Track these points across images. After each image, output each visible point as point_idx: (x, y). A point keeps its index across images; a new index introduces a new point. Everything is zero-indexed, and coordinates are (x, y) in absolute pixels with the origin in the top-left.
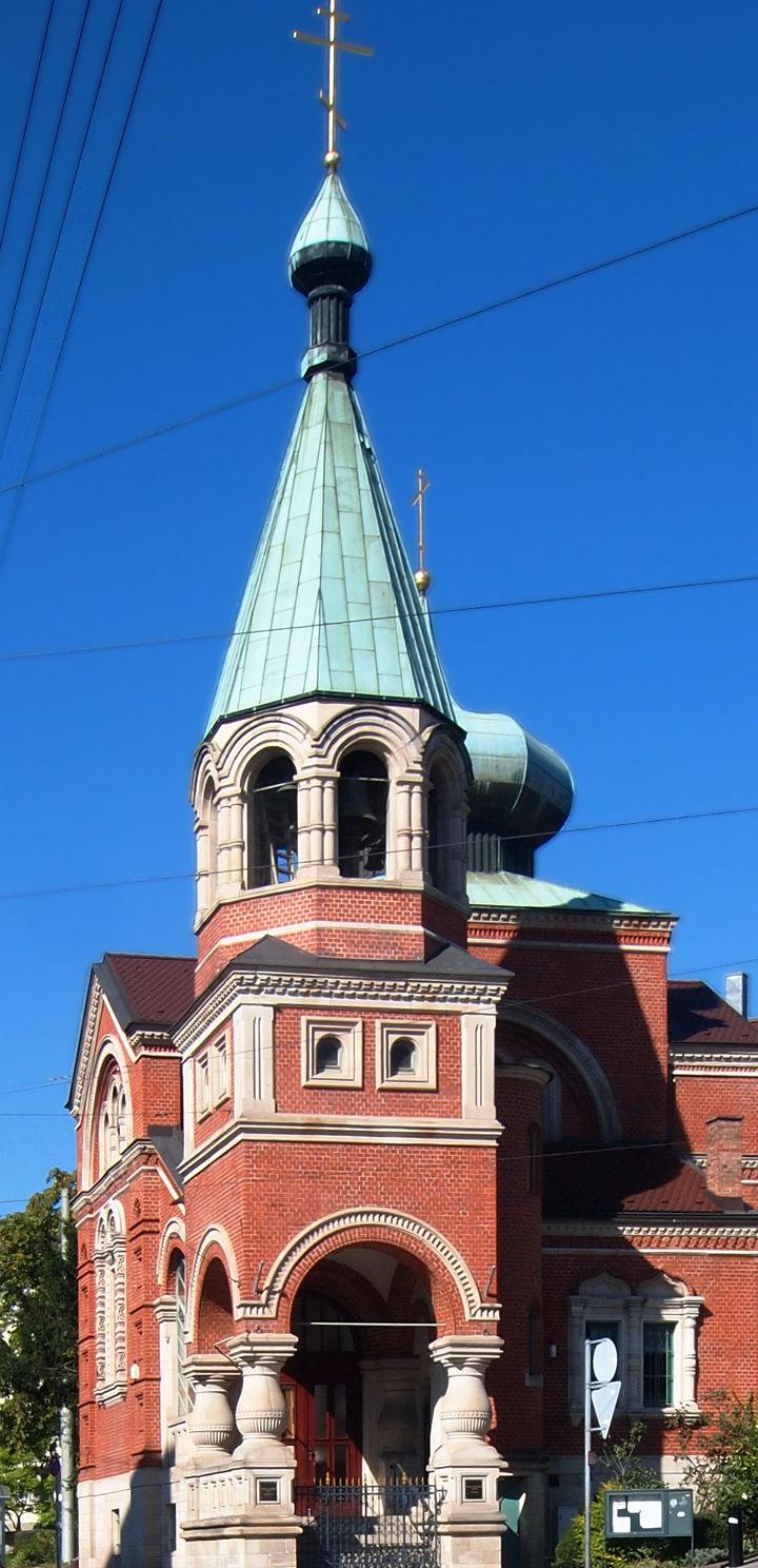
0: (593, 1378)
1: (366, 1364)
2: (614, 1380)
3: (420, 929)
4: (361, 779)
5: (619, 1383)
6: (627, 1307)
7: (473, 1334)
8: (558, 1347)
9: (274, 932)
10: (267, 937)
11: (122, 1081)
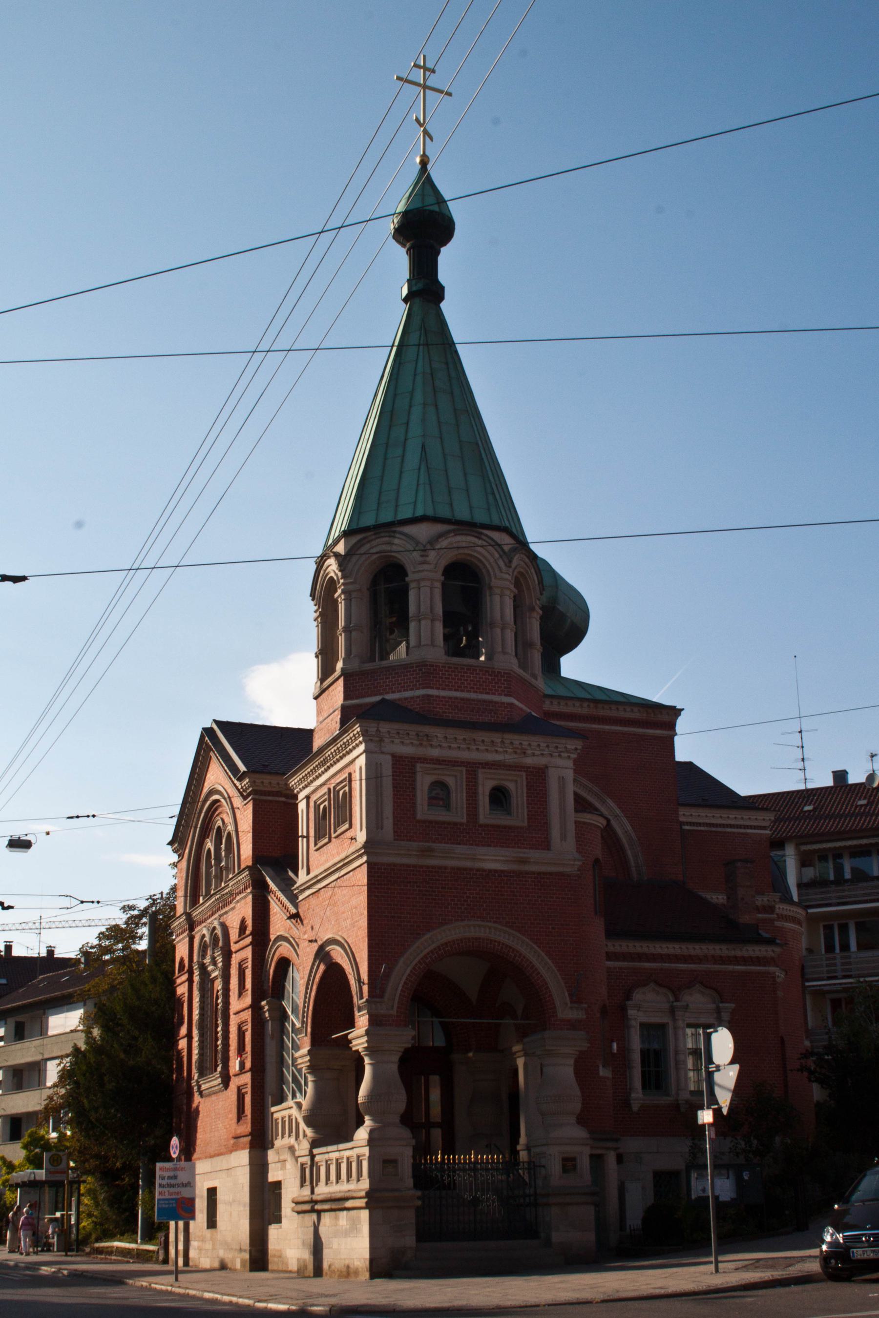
2: (732, 1062)
5: (737, 1067)
6: (672, 1011)
8: (618, 1044)
9: (389, 697)
10: (383, 699)
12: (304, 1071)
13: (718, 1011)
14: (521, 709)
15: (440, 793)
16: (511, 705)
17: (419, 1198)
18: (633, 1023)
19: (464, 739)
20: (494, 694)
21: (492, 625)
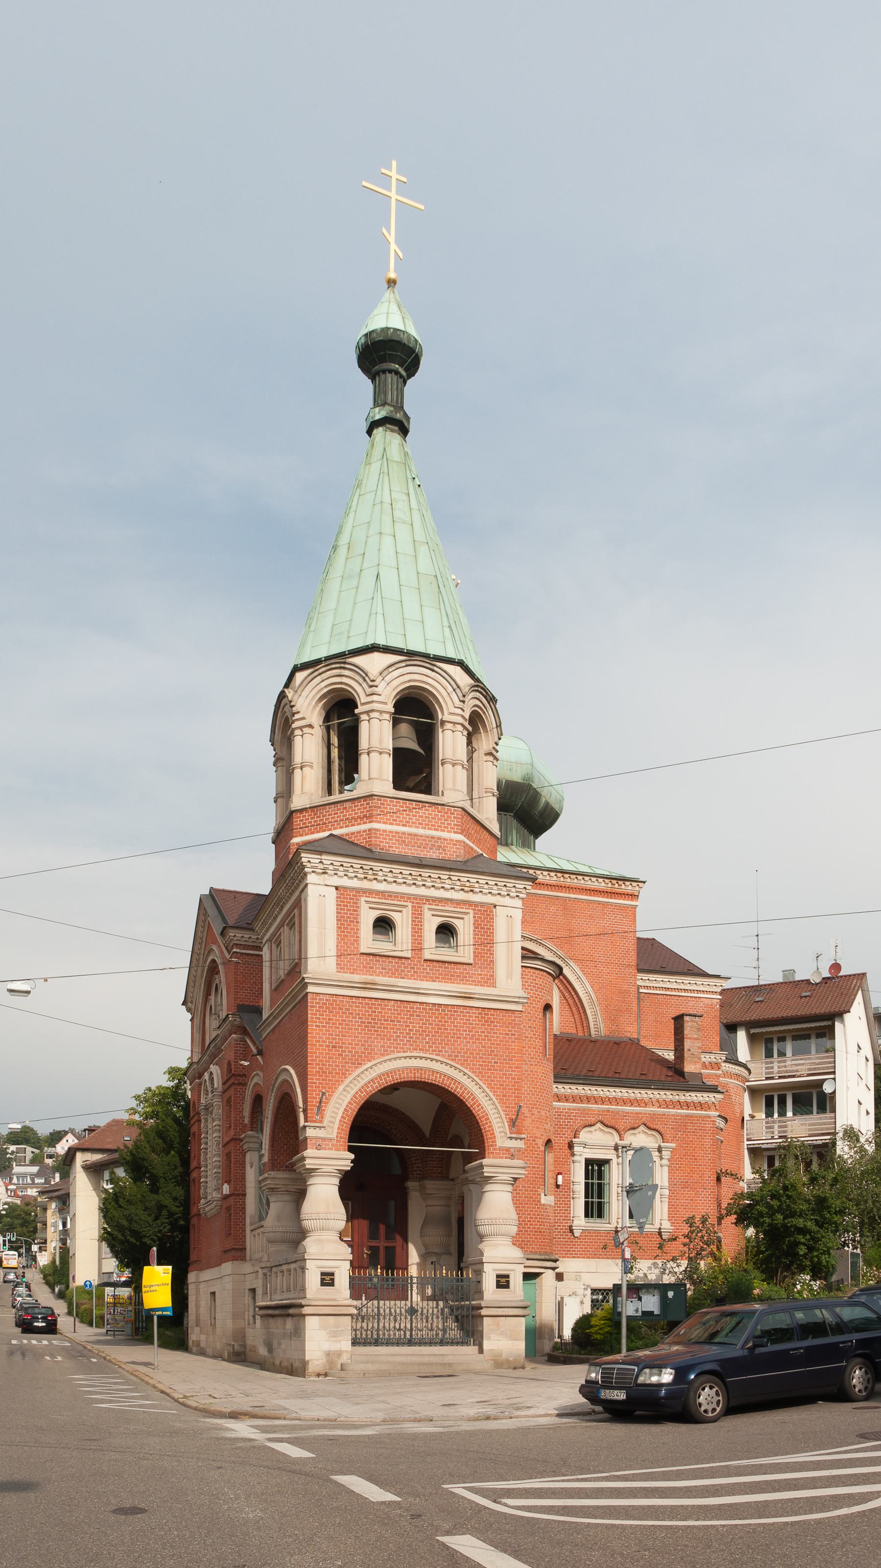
1: (410, 1184)
4: (374, 1493)
7: (502, 1158)
9: (336, 832)
11: (222, 978)
20: (443, 831)
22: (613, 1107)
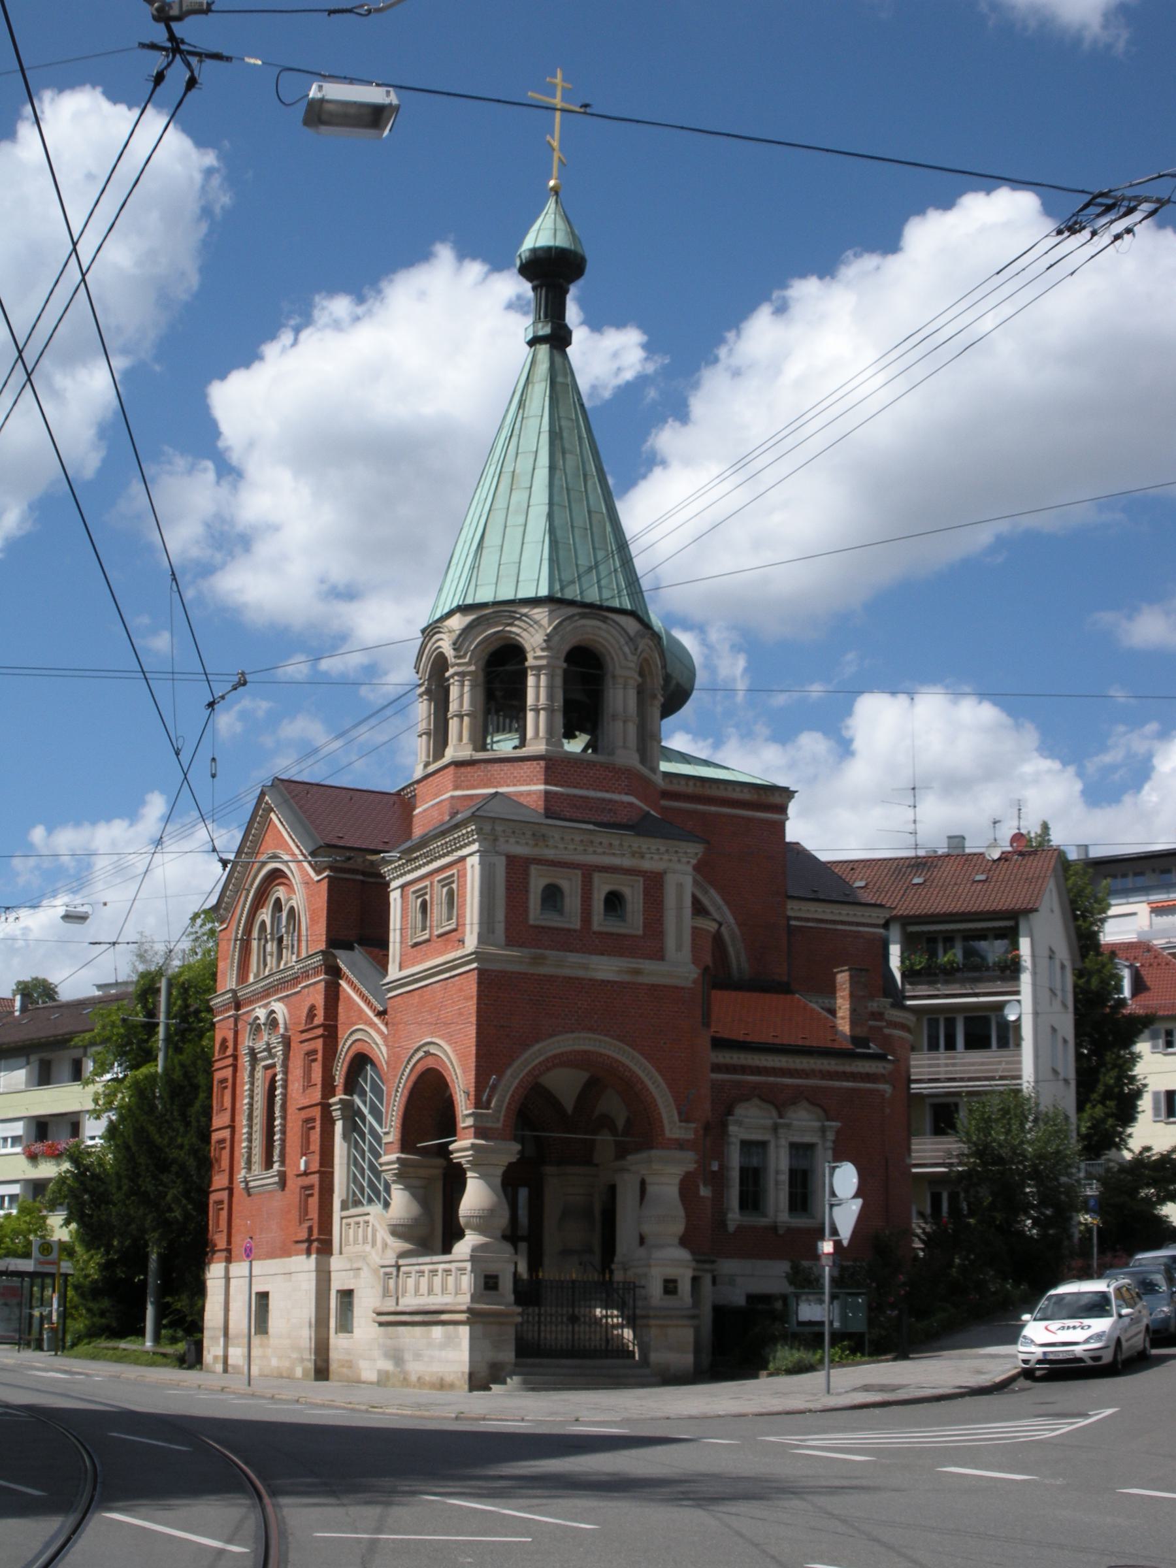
0: (833, 1194)
3: (542, 787)
5: (859, 1201)
6: (775, 1128)
9: (501, 790)
12: (388, 1177)
13: (823, 1130)
14: (640, 808)
15: (552, 896)
16: (631, 804)
17: (519, 1314)
18: (733, 1140)
19: (582, 841)
21: (614, 717)
22: (771, 1079)
